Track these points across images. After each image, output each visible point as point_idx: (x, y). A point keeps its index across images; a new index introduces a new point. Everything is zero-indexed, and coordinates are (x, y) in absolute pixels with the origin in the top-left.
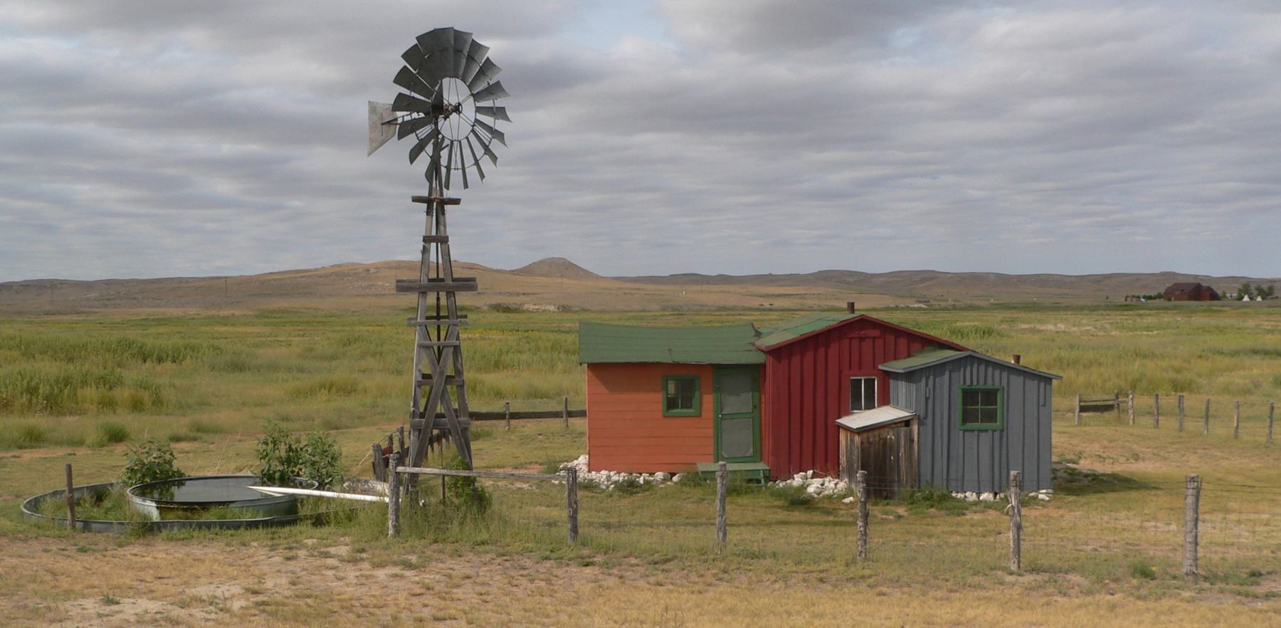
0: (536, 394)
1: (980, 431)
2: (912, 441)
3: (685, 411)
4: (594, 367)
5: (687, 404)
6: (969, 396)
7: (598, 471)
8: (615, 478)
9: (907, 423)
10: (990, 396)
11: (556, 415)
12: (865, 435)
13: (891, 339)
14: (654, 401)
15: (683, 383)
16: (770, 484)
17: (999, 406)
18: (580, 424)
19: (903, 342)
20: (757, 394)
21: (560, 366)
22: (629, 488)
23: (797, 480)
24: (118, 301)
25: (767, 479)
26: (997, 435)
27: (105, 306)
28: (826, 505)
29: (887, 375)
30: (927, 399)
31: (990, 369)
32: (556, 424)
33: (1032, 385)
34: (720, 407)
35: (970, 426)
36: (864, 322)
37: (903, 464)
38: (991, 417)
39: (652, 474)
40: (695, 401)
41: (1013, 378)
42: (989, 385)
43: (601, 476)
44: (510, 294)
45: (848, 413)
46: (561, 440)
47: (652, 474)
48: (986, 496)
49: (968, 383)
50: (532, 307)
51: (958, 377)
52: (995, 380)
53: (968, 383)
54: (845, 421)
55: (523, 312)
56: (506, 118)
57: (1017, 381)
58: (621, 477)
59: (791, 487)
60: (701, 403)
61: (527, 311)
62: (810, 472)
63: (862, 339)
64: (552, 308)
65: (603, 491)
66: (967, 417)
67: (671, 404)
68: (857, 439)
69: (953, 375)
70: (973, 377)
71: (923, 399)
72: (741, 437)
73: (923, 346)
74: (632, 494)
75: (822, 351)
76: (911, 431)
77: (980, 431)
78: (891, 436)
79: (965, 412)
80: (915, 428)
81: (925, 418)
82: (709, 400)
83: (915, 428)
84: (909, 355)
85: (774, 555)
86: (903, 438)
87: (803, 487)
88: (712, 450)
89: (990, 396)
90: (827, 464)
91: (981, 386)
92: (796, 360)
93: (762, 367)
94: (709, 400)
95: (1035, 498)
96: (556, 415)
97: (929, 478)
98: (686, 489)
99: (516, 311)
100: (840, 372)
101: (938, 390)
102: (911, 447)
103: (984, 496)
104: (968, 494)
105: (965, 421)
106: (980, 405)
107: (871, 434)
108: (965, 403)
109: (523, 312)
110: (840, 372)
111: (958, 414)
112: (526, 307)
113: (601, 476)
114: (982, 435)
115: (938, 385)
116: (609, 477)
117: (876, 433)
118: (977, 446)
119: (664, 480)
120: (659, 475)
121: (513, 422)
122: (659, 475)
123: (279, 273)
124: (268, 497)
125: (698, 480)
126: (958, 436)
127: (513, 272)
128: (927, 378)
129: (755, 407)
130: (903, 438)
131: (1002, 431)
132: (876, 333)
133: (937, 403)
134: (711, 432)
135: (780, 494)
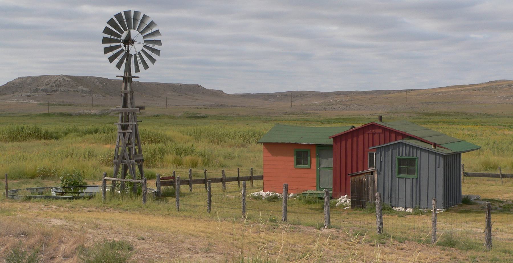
3: (304, 165)
6: (401, 162)
10: (412, 162)
14: (292, 160)
15: (302, 153)
17: (416, 167)
24: (334, 106)
26: (414, 180)
27: (325, 109)
30: (381, 162)
35: (402, 176)
36: (371, 127)
41: (423, 153)
42: (411, 157)
48: (409, 210)
52: (414, 154)
56: (158, 54)
63: (374, 134)
67: (298, 163)
76: (374, 178)
78: (364, 179)
80: (376, 175)
81: (381, 171)
82: (314, 161)
83: (376, 175)
85: (420, 241)
86: (370, 180)
88: (315, 184)
91: (407, 157)
94: (314, 161)
103: (409, 210)
104: (400, 208)
105: (399, 173)
108: (399, 164)
110: (364, 149)
111: (396, 170)
114: (407, 180)
115: (386, 156)
117: (358, 177)
121: (504, 179)
123: (448, 87)
128: (381, 152)
130: (370, 180)
132: (380, 131)
133: (386, 164)
134: (315, 176)
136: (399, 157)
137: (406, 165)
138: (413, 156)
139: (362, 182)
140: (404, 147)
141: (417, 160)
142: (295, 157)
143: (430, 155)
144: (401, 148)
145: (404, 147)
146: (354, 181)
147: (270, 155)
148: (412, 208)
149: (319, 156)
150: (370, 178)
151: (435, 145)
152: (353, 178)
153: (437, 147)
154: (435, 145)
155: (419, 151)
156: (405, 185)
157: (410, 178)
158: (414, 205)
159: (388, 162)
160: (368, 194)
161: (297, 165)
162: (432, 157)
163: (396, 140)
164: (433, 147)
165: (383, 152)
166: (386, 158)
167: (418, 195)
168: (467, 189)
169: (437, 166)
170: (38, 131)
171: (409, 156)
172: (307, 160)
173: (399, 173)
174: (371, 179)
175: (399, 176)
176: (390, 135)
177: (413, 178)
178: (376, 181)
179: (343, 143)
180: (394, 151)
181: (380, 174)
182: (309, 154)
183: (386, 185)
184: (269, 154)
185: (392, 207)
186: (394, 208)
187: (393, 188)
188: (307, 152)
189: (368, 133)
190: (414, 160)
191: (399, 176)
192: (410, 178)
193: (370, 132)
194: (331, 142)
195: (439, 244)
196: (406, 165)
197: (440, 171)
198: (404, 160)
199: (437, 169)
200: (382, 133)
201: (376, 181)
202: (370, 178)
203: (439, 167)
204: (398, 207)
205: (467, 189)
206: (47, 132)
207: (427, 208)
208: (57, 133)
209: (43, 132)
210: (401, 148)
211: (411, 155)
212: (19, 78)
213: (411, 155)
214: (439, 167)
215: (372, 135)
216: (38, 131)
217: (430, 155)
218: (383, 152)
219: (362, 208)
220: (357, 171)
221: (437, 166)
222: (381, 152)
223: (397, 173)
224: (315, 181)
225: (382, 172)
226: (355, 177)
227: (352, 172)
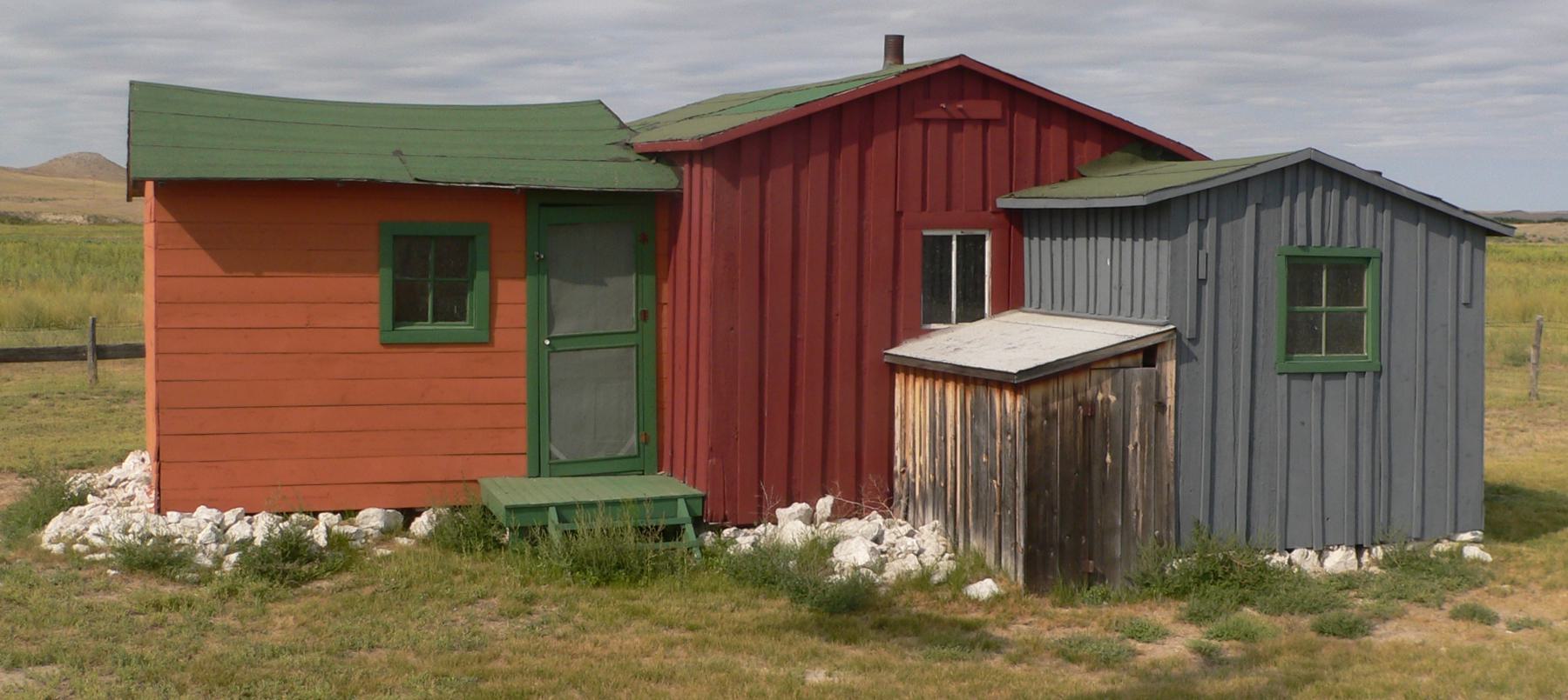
0: (40, 322)
1: (1327, 375)
2: (1161, 407)
4: (174, 192)
5: (452, 309)
6: (1302, 273)
7: (187, 508)
8: (239, 531)
9: (1149, 355)
10: (1349, 273)
11: (73, 354)
12: (1037, 392)
13: (1026, 125)
14: (364, 293)
16: (708, 537)
18: (143, 375)
19: (1056, 137)
20: (649, 280)
21: (85, 280)
22: (286, 563)
23: (791, 526)
25: (699, 524)
28: (921, 605)
29: (1020, 223)
30: (1201, 282)
31: (1351, 203)
32: (72, 375)
33: (1445, 245)
34: (544, 315)
35: (1304, 360)
36: (963, 77)
37: (1135, 474)
38: (1346, 336)
39: (348, 514)
40: (475, 301)
43: (196, 525)
44: (21, 199)
45: (917, 332)
46: (82, 407)
47: (348, 514)
49: (1301, 239)
50: (51, 218)
51: (1277, 221)
52: (1364, 229)
53: (1301, 239)
54: (911, 349)
55: (39, 223)
57: (1412, 234)
58: (261, 528)
59: (777, 549)
60: (492, 304)
61: (45, 222)
62: (825, 504)
63: (956, 124)
64: (79, 219)
65: (206, 577)
66: (1299, 336)
67: (405, 309)
68: (1009, 405)
69: (1226, 228)
70: (1314, 222)
71: (1190, 282)
72: (601, 401)
73: (1106, 151)
74: (298, 581)
75: (850, 152)
76: (1159, 378)
77: (1327, 375)
78: (1105, 394)
79: (1292, 323)
80: (1170, 368)
81: (1195, 340)
82: (514, 295)
83: (1170, 368)
84: (1072, 174)
87: (821, 551)
88: (520, 441)
89: (1349, 273)
90: (868, 481)
91: (1331, 248)
92: (781, 178)
93: (667, 204)
94: (514, 295)
95: (1456, 555)
96: (73, 354)
97: (1202, 516)
98: (465, 562)
99: (28, 222)
100: (898, 215)
101: (1225, 257)
102: (1158, 426)
104: (1297, 555)
105: (1292, 346)
106: (1324, 298)
107: (1052, 387)
108: (1292, 299)
109: (39, 223)
110: (898, 215)
112: (43, 217)
113: (196, 525)
114: (1331, 385)
116: (221, 530)
117: (1068, 383)
118: (1322, 419)
119: (387, 534)
120: (372, 519)
122: (372, 519)
124: (426, 295)
125: (476, 530)
126: (1275, 389)
127: (25, 171)
128: (1203, 223)
129: (644, 315)
131: (1378, 374)
132: (991, 108)
134: (519, 389)
135: (764, 572)
139: (1089, 418)
142: (387, 273)
147: (218, 271)
149: (540, 265)
174: (1145, 392)
176: (1038, 133)
178: (1170, 402)
184: (202, 262)
195: (580, 565)
201: (1170, 402)
202: (1137, 385)
215: (943, 129)
218: (1212, 222)
219: (1093, 579)
224: (522, 417)
225: (1204, 349)
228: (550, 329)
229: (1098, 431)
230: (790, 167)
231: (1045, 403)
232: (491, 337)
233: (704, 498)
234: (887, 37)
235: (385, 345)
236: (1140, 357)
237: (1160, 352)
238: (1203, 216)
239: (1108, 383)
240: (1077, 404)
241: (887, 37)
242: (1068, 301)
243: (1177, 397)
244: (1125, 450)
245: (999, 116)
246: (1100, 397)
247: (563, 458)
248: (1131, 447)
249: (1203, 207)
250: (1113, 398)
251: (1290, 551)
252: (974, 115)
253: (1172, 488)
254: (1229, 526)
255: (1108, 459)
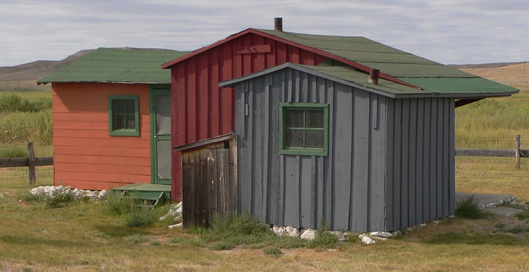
2: (231, 164)
10: (316, 115)
14: (105, 117)
26: (321, 161)
30: (246, 118)
35: (293, 150)
36: (249, 38)
42: (313, 105)
48: (309, 234)
52: (321, 98)
63: (253, 56)
67: (118, 123)
76: (230, 154)
80: (235, 149)
81: (246, 138)
82: (147, 120)
83: (235, 149)
86: (222, 161)
88: (148, 171)
104: (288, 229)
105: (286, 145)
108: (287, 122)
114: (288, 159)
117: (197, 153)
128: (246, 94)
130: (222, 161)
132: (267, 48)
133: (258, 122)
134: (148, 152)
136: (287, 105)
137: (301, 123)
138: (318, 101)
139: (205, 166)
140: (298, 80)
141: (326, 111)
142: (110, 112)
143: (357, 98)
144: (290, 83)
145: (298, 80)
146: (190, 164)
147: (66, 110)
148: (315, 228)
149: (156, 110)
150: (222, 155)
151: (376, 75)
152: (186, 156)
153: (380, 81)
154: (376, 75)
155: (331, 90)
156: (298, 173)
157: (309, 157)
158: (319, 223)
159: (263, 117)
160: (218, 194)
161: (114, 128)
162: (362, 103)
163: (277, 64)
164: (370, 81)
165: (251, 93)
166: (258, 109)
167: (329, 199)
168: (471, 178)
169: (374, 125)
170: (16, 101)
171: (309, 101)
172: (133, 118)
173: (286, 145)
174: (224, 158)
175: (286, 152)
177: (317, 157)
178: (236, 163)
179: (192, 78)
180: (275, 90)
181: (244, 146)
182: (136, 107)
183: (258, 173)
185: (272, 226)
186: (275, 229)
187: (274, 181)
188: (134, 100)
189: (242, 55)
190: (321, 111)
191: (286, 152)
192: (309, 157)
193: (246, 51)
194: (166, 77)
196: (301, 123)
197: (380, 137)
198: (299, 111)
199: (374, 132)
200: (271, 53)
201: (236, 163)
202: (222, 155)
203: (377, 128)
204: (284, 225)
205: (471, 178)
206: (27, 103)
207: (349, 229)
208: (41, 104)
209: (22, 103)
210: (290, 83)
211: (314, 100)
212: (81, 52)
213: (314, 100)
214: (377, 128)
215: (249, 57)
216: (16, 101)
217: (357, 98)
218: (251, 93)
220: (198, 139)
221: (374, 125)
222: (246, 94)
223: (281, 145)
226: (191, 154)
227: (187, 141)
228: (157, 131)
229: (209, 171)
230: (195, 74)
231: (189, 159)
232: (140, 134)
233: (170, 192)
234: (275, 19)
235: (111, 136)
236: (223, 145)
237: (230, 143)
238: (247, 91)
239: (210, 154)
240: (200, 161)
241: (275, 19)
242: (226, 123)
243: (238, 161)
244: (218, 179)
245: (270, 51)
246: (208, 159)
247: (161, 178)
248: (221, 179)
249: (247, 89)
250: (213, 160)
251: (286, 227)
252: (260, 51)
253: (236, 196)
254: (261, 213)
255: (213, 182)
